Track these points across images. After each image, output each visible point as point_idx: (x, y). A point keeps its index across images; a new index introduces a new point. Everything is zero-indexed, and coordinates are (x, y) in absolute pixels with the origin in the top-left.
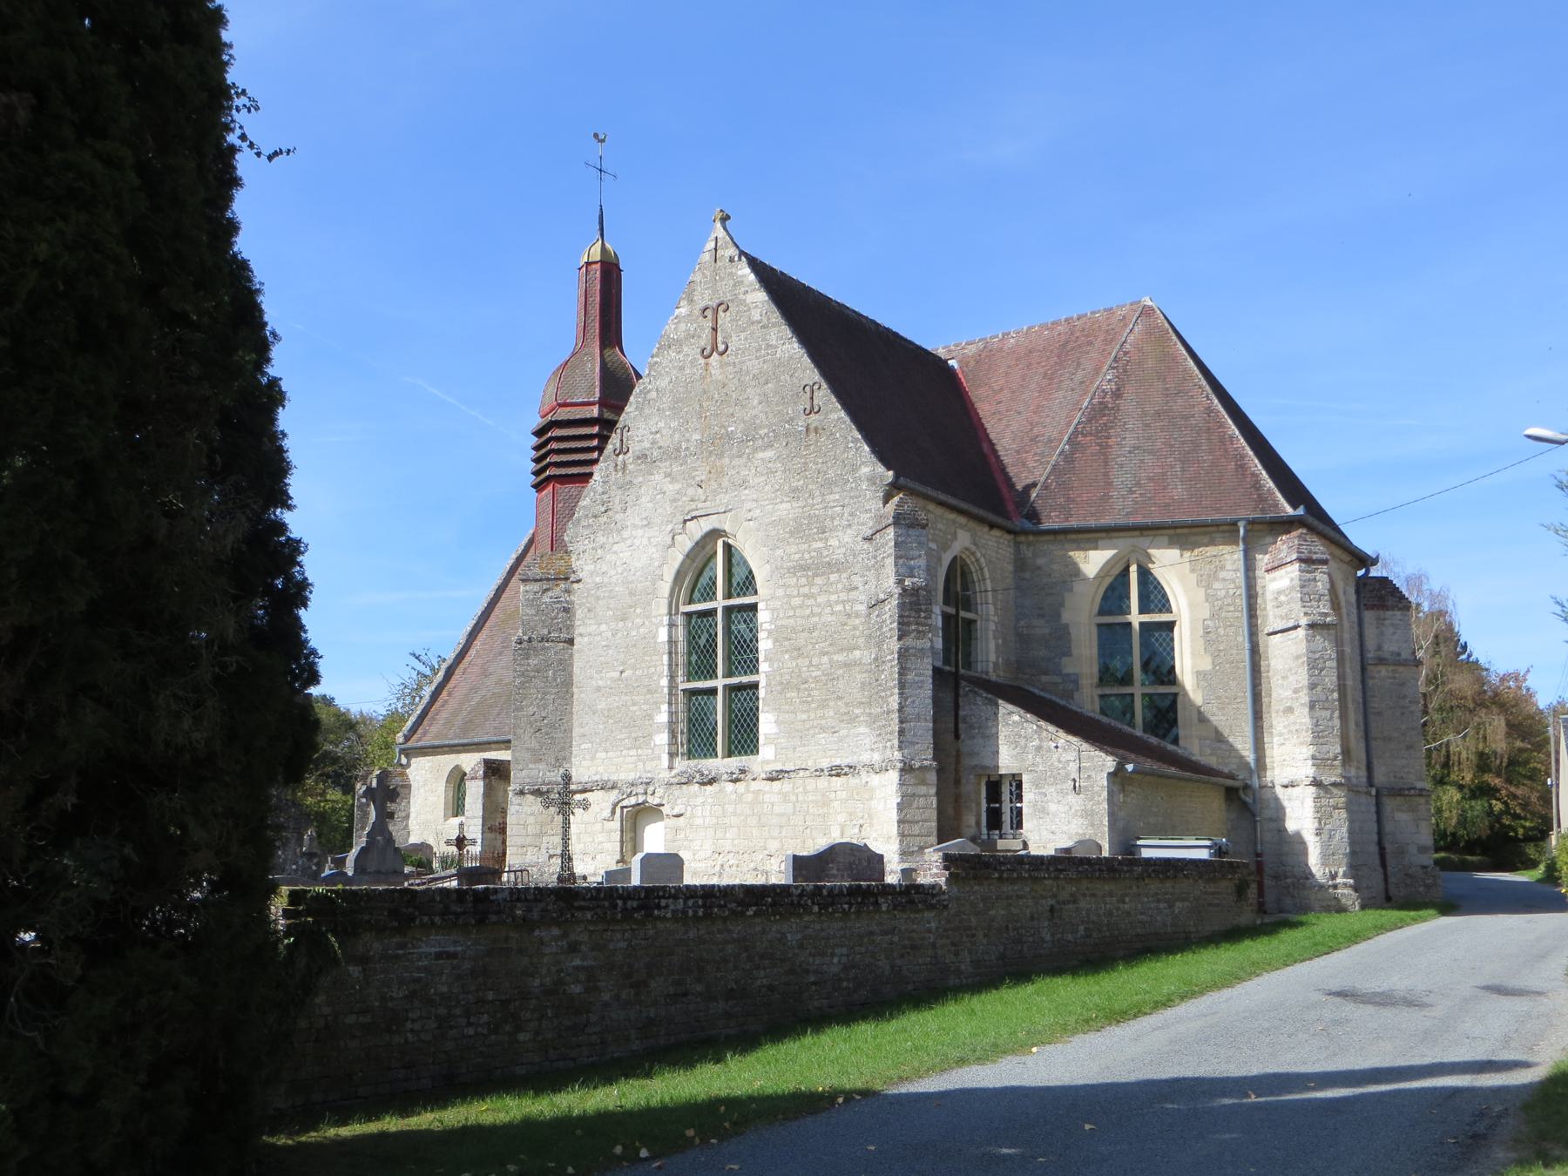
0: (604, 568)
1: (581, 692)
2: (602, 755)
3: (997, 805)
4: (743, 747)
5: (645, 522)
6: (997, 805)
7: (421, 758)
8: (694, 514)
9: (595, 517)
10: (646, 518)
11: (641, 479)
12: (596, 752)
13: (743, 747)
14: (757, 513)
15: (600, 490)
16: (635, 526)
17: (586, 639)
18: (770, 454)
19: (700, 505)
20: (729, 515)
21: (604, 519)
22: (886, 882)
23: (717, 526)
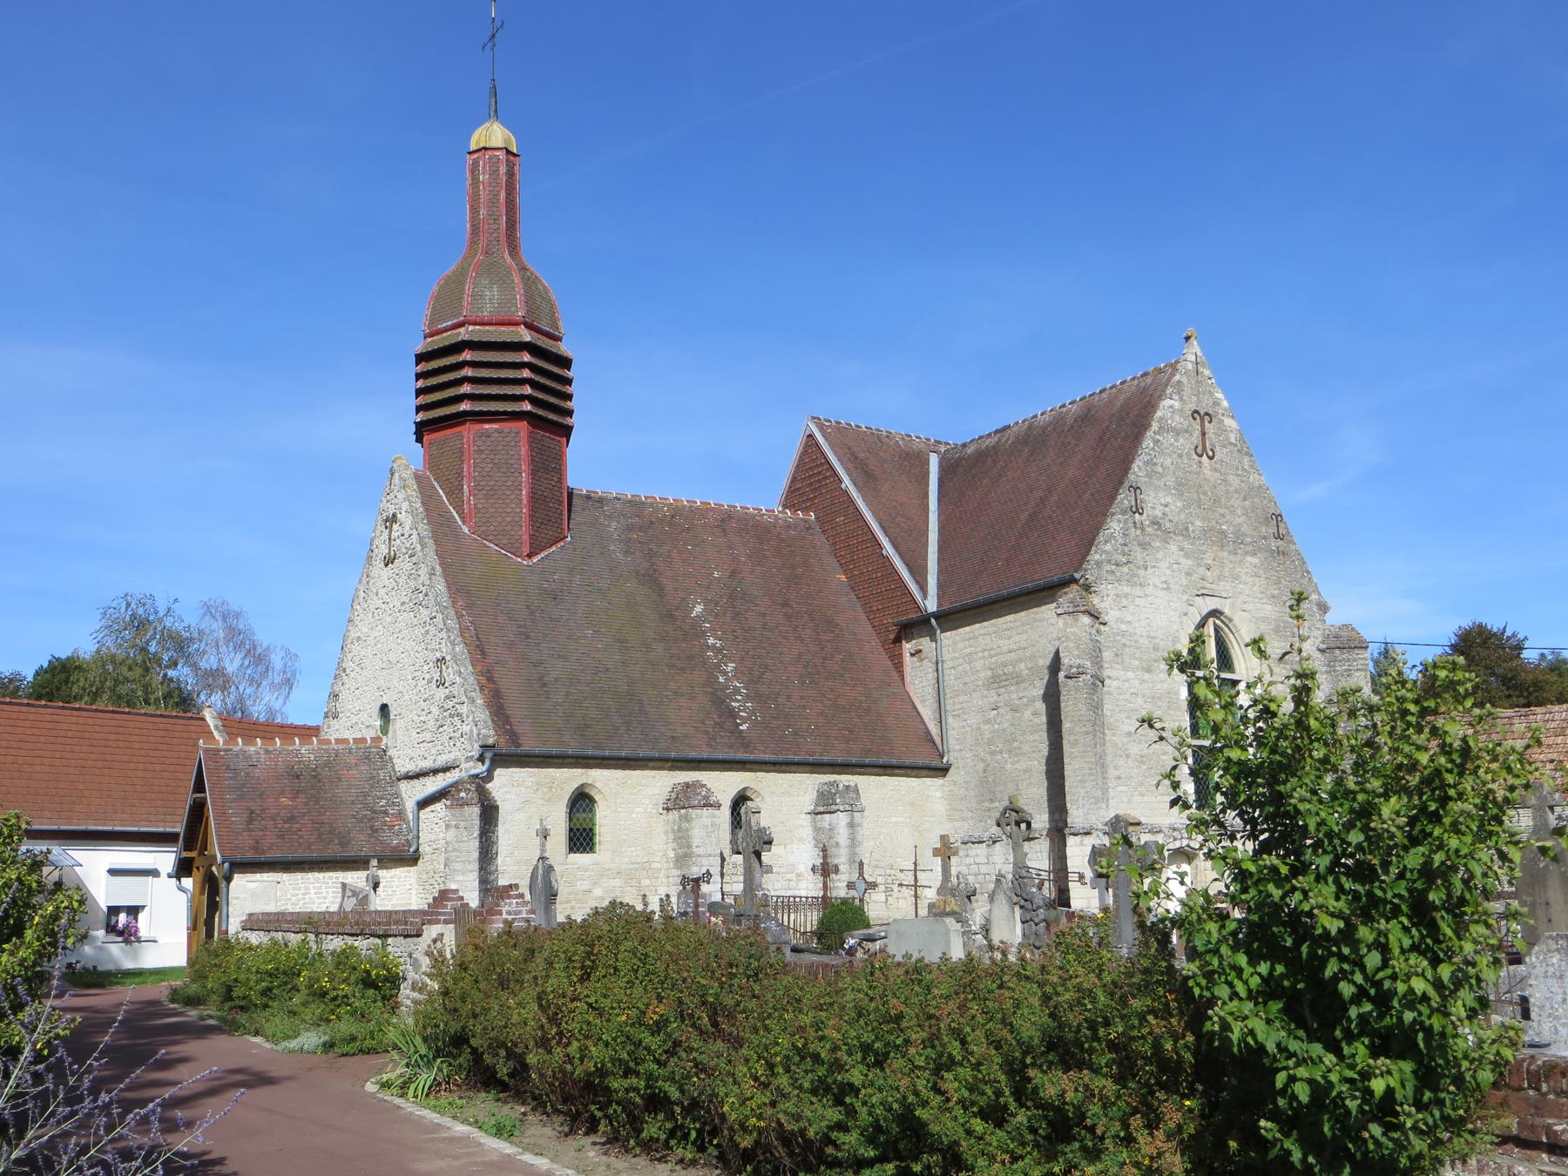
0: (1129, 618)
1: (1114, 735)
2: (1138, 799)
3: (934, 461)
4: (581, 844)
5: (1165, 586)
6: (934, 461)
7: (518, 770)
8: (1205, 591)
9: (1117, 565)
10: (1165, 582)
11: (1158, 544)
12: (1132, 795)
13: (581, 844)
14: (1250, 607)
15: (1121, 541)
16: (1155, 586)
17: (1115, 683)
18: (1255, 560)
19: (1208, 585)
20: (1228, 601)
21: (1126, 569)
22: (1371, 1084)
23: (1220, 608)
